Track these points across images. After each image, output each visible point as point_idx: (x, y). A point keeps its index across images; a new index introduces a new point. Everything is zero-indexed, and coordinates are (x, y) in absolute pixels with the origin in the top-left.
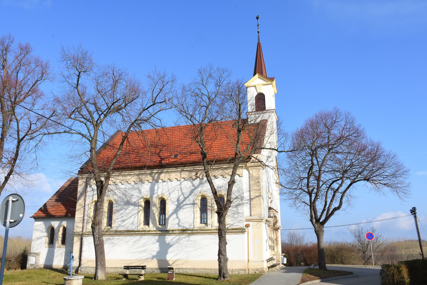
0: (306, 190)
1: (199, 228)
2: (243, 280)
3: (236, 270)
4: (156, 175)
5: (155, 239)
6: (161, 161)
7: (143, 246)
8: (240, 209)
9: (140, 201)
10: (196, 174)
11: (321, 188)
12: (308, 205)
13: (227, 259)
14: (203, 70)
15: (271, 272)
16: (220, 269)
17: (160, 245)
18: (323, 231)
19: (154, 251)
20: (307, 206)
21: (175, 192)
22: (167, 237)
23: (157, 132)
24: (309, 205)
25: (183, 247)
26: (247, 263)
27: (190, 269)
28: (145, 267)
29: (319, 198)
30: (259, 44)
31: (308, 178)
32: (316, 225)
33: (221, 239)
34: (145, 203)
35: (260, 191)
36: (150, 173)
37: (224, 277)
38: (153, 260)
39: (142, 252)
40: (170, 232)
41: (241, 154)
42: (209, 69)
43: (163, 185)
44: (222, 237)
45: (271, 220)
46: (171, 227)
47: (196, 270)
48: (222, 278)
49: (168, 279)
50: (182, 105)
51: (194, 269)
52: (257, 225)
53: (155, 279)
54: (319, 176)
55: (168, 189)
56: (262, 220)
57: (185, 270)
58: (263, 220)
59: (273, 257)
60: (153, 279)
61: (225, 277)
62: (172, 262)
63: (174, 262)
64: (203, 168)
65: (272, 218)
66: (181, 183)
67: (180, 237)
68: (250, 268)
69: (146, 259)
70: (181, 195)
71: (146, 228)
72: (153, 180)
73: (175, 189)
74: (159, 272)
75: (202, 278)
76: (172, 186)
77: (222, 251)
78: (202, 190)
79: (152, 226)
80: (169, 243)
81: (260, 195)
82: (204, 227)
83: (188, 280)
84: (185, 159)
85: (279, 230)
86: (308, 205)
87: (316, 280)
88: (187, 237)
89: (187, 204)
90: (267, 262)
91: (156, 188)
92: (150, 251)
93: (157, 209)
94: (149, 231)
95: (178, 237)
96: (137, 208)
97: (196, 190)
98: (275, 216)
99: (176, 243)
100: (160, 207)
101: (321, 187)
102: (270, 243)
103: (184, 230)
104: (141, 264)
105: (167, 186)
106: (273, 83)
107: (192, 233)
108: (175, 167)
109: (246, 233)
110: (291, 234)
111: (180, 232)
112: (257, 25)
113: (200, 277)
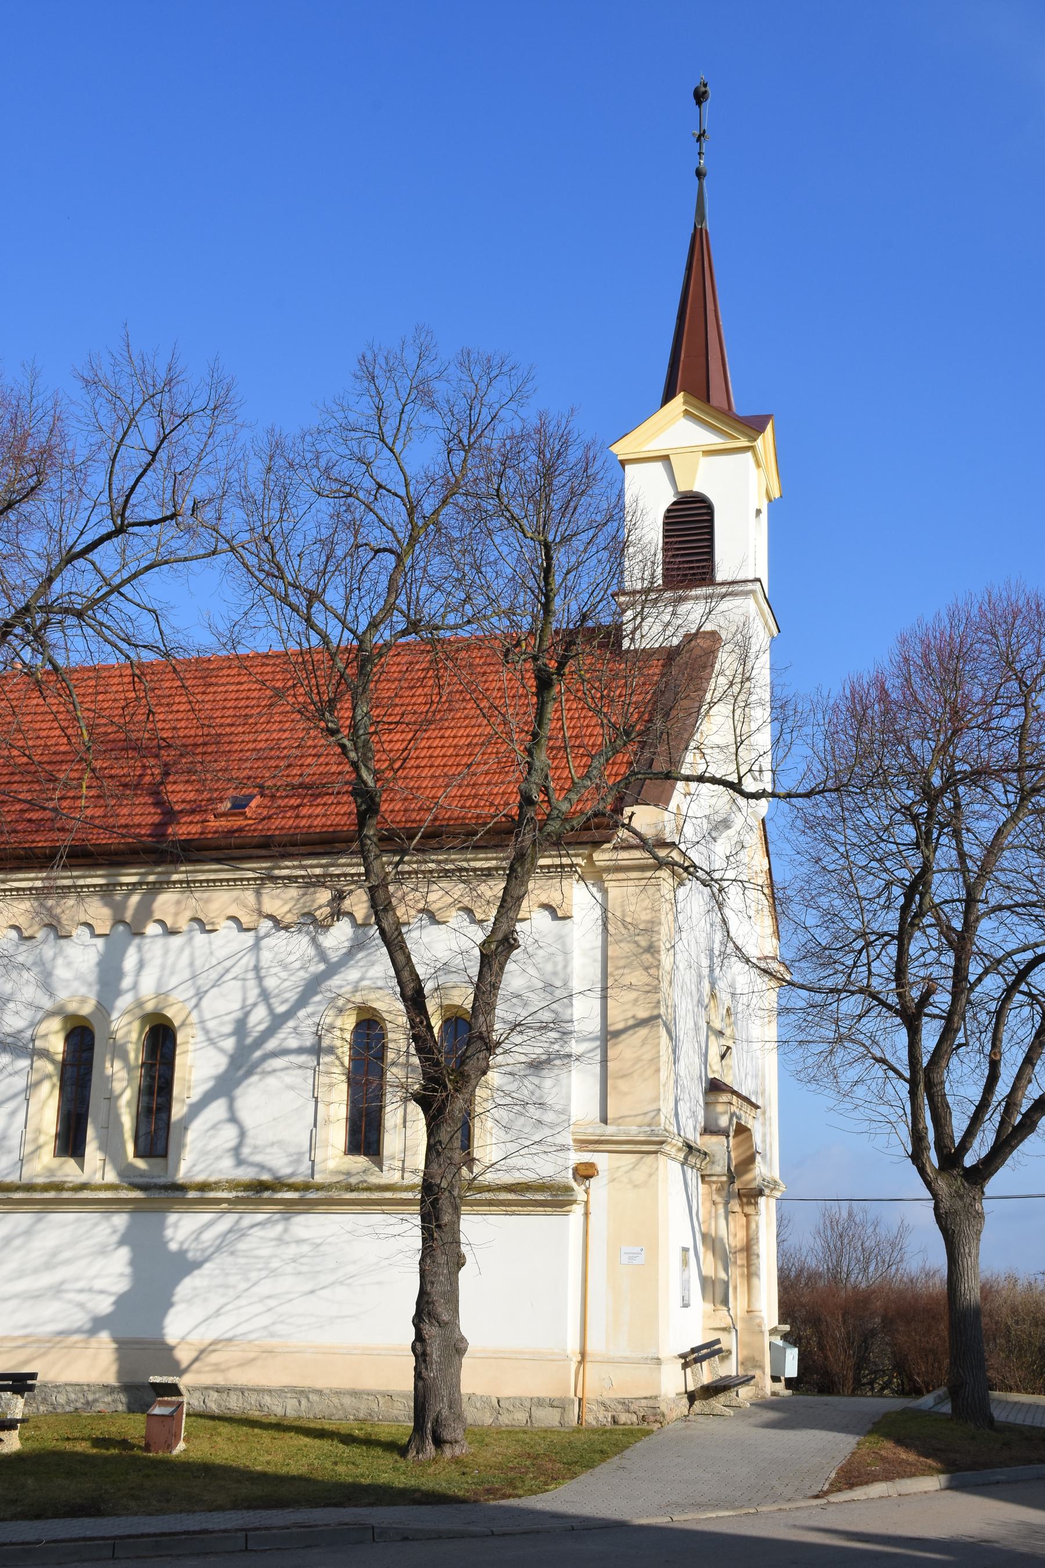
0: (893, 1000)
1: (341, 1178)
2: (537, 1457)
3: (519, 1402)
4: (135, 899)
5: (109, 1231)
6: (164, 824)
7: (49, 1266)
8: (548, 1083)
9: (43, 1029)
10: (333, 899)
11: (978, 989)
12: (900, 1076)
13: (462, 1346)
14: (381, 360)
15: (700, 1419)
16: (421, 1400)
17: (133, 1263)
18: (980, 1216)
19: (101, 1292)
20: (895, 1082)
21: (225, 988)
22: (172, 1218)
23: (138, 673)
24: (907, 1074)
25: (254, 1276)
26: (573, 1366)
27: (280, 1392)
28: (30, 1382)
29: (966, 1044)
30: (698, 242)
31: (902, 938)
32: (941, 1184)
33: (433, 1239)
34: (67, 1039)
35: (655, 997)
36: (101, 886)
37: (439, 1442)
38: (94, 1342)
39: (36, 1296)
40: (192, 1195)
41: (553, 800)
42: (411, 358)
43: (166, 952)
44: (439, 1226)
45: (715, 1144)
46: (197, 1169)
47: (311, 1396)
48: (430, 1448)
49: (147, 1448)
50: (266, 539)
51: (301, 1393)
52: (633, 1168)
53: (82, 1447)
54: (969, 925)
55: (193, 972)
56: (662, 1143)
57: (253, 1398)
58: (667, 1148)
59: (718, 1341)
60: (68, 1446)
61: (446, 1442)
62: (194, 1354)
63: (202, 1352)
64: (362, 870)
65: (724, 1138)
66: (258, 939)
67: (240, 1218)
68: (588, 1395)
69: (61, 1333)
70: (255, 1005)
71: (69, 1170)
72: (118, 921)
73: (227, 971)
74: (121, 1408)
75: (325, 1445)
76: (211, 953)
77: (433, 1302)
78: (362, 979)
79: (100, 1163)
80: (182, 1253)
81: (655, 1013)
82: (364, 1172)
83: (250, 1451)
84: (283, 818)
85: (762, 1200)
86: (900, 1076)
87: (922, 1478)
88: (277, 1221)
89: (285, 1052)
90: (685, 1366)
91: (130, 962)
92: (81, 1291)
93: (129, 1073)
94: (84, 1187)
95: (229, 1220)
96: (24, 1063)
97: (335, 981)
98: (742, 1130)
99: (218, 1249)
100: (143, 1064)
101: (974, 985)
102: (710, 1266)
103: (260, 1186)
104: (26, 1362)
105: (187, 953)
106: (759, 443)
107: (301, 1201)
108: (218, 861)
109: (578, 1210)
110: (833, 1223)
111: (240, 1194)
112: (697, 133)
113: (321, 1434)
